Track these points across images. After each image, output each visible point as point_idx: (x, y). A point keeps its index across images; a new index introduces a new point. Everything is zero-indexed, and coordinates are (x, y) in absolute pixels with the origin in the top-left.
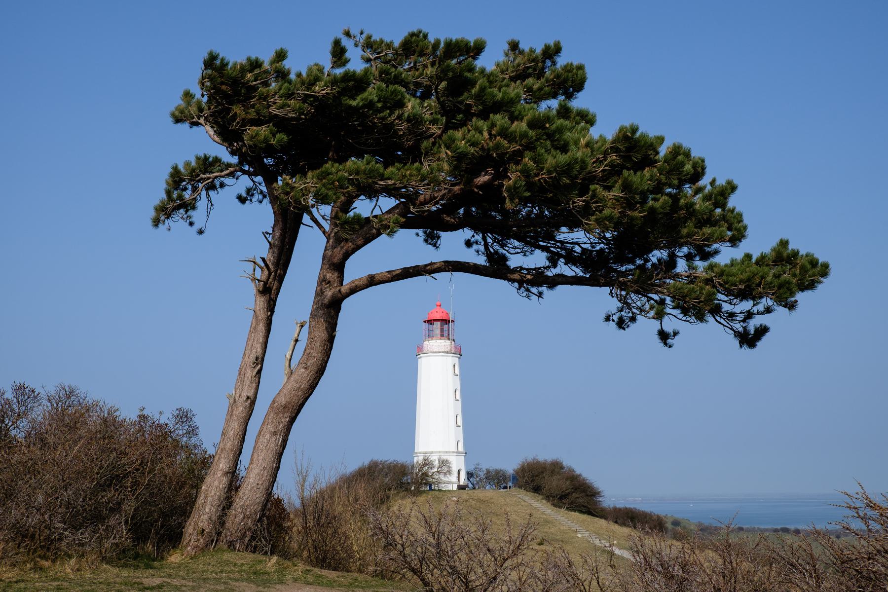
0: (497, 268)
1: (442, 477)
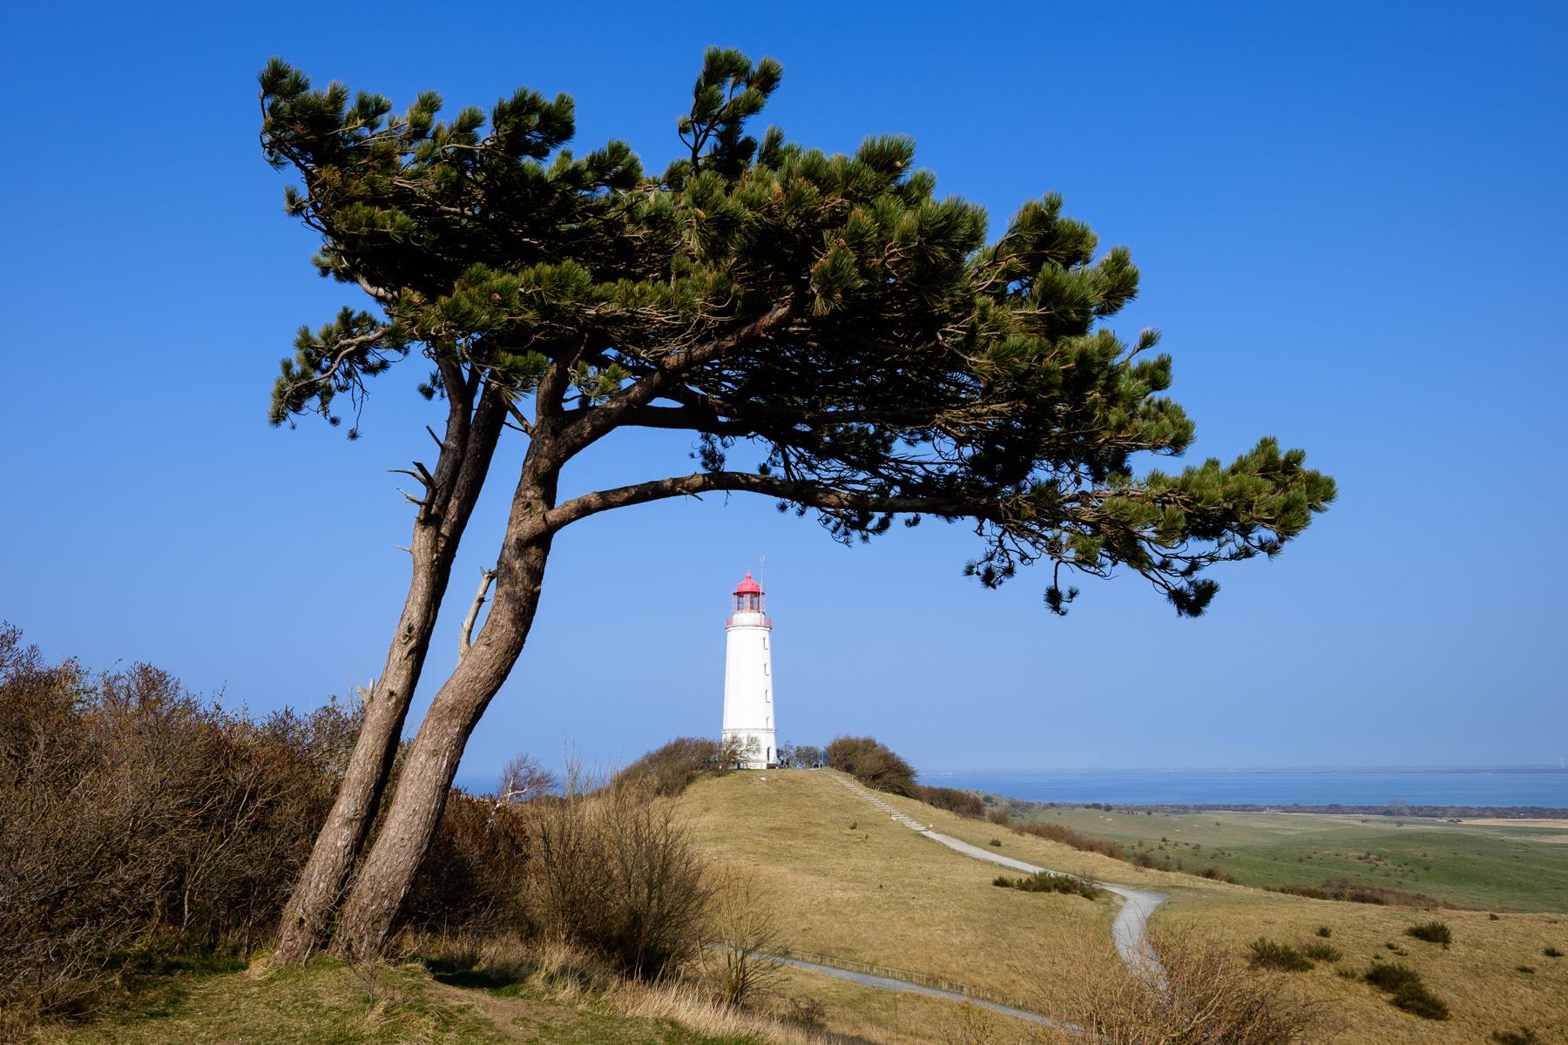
1: (751, 755)
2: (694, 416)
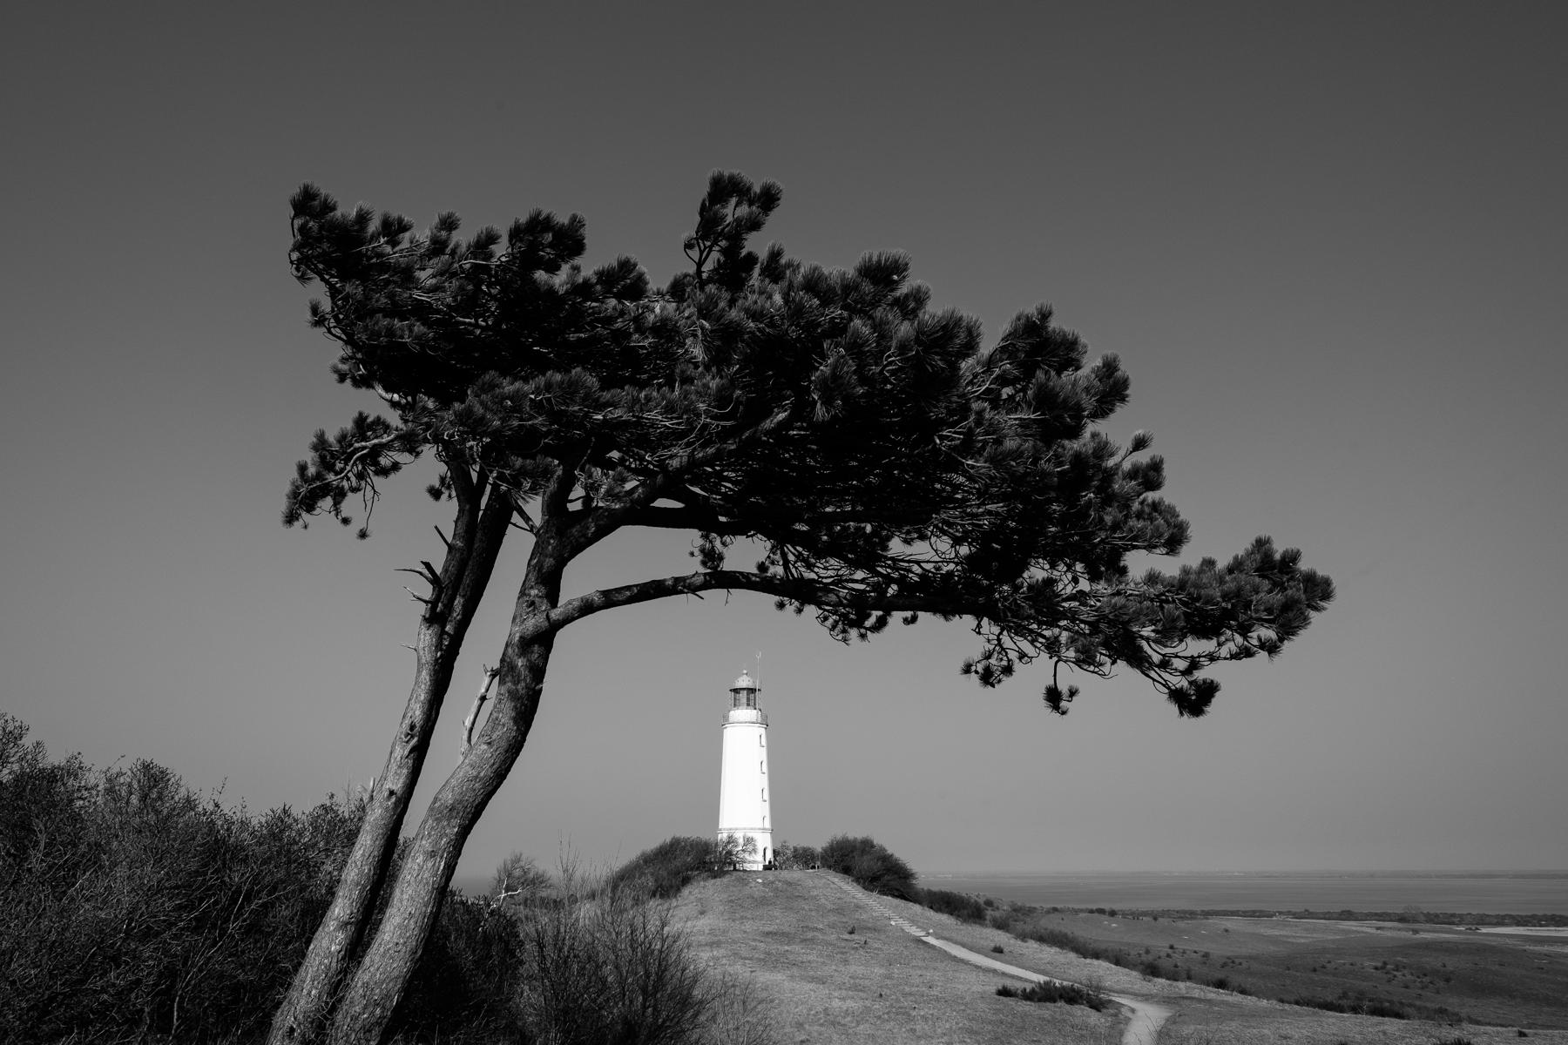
0: (799, 592)
1: (747, 856)
2: (694, 516)
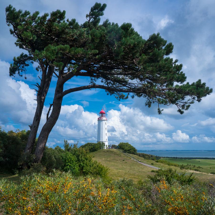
2: (90, 74)
